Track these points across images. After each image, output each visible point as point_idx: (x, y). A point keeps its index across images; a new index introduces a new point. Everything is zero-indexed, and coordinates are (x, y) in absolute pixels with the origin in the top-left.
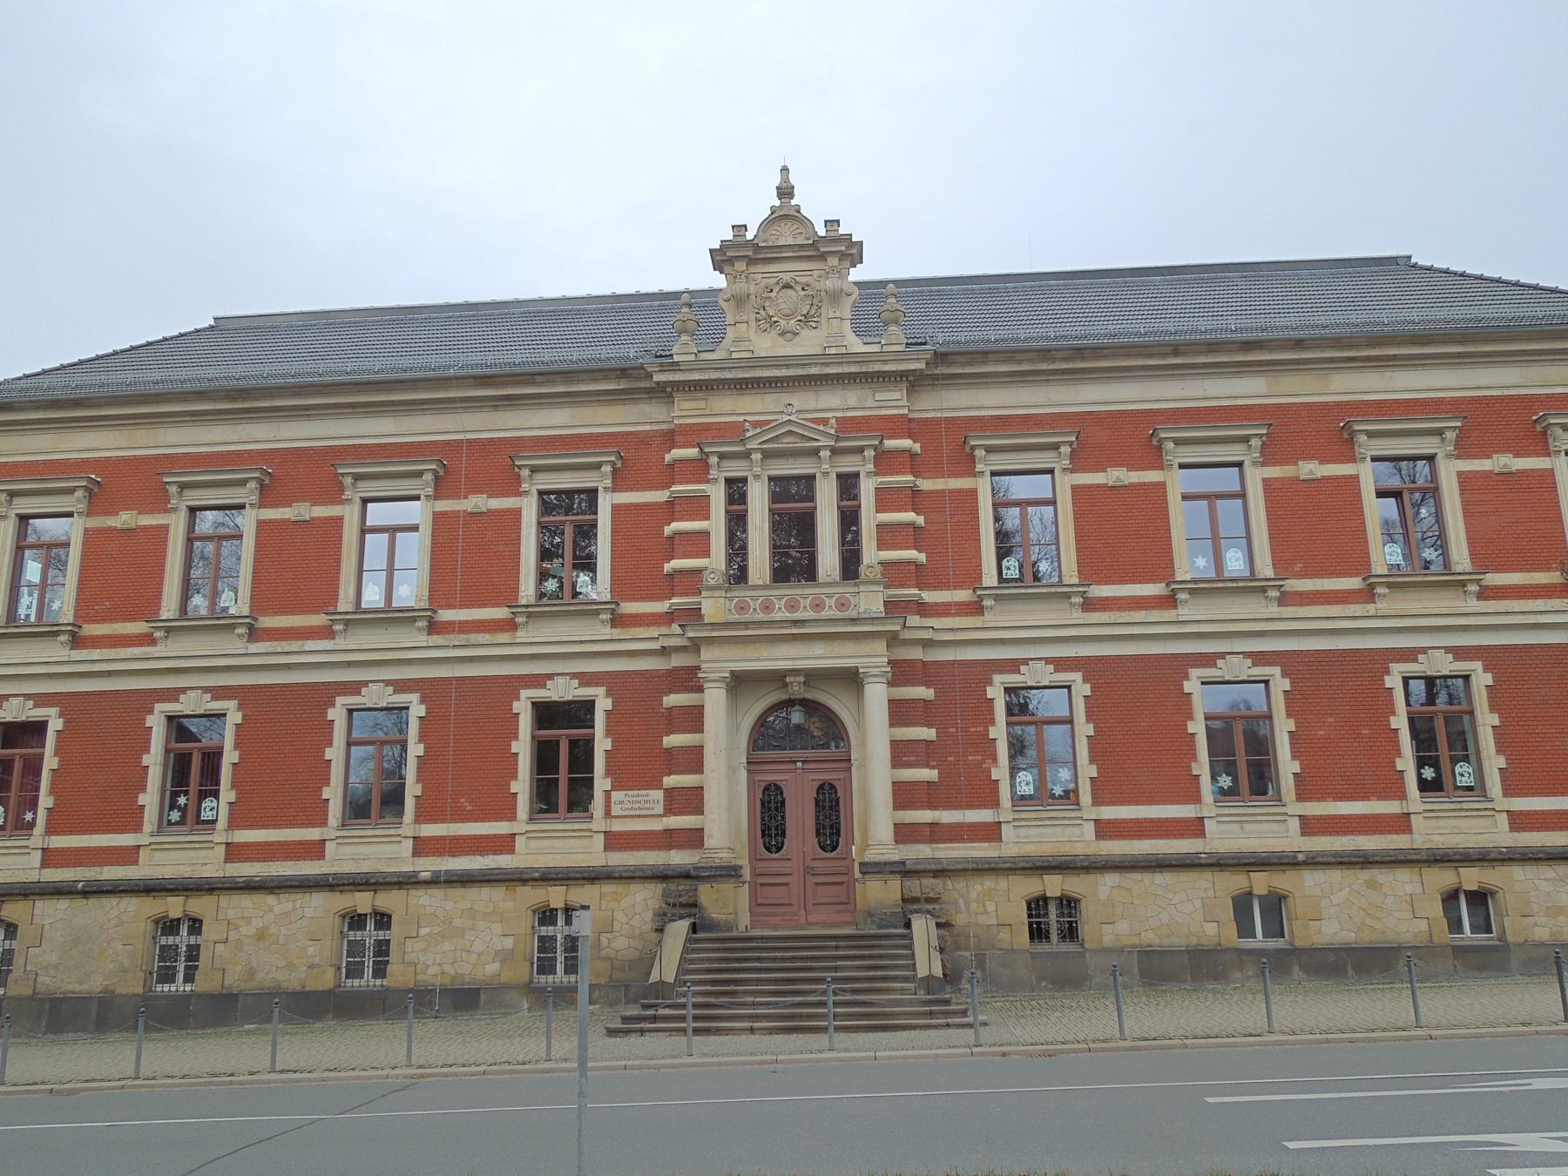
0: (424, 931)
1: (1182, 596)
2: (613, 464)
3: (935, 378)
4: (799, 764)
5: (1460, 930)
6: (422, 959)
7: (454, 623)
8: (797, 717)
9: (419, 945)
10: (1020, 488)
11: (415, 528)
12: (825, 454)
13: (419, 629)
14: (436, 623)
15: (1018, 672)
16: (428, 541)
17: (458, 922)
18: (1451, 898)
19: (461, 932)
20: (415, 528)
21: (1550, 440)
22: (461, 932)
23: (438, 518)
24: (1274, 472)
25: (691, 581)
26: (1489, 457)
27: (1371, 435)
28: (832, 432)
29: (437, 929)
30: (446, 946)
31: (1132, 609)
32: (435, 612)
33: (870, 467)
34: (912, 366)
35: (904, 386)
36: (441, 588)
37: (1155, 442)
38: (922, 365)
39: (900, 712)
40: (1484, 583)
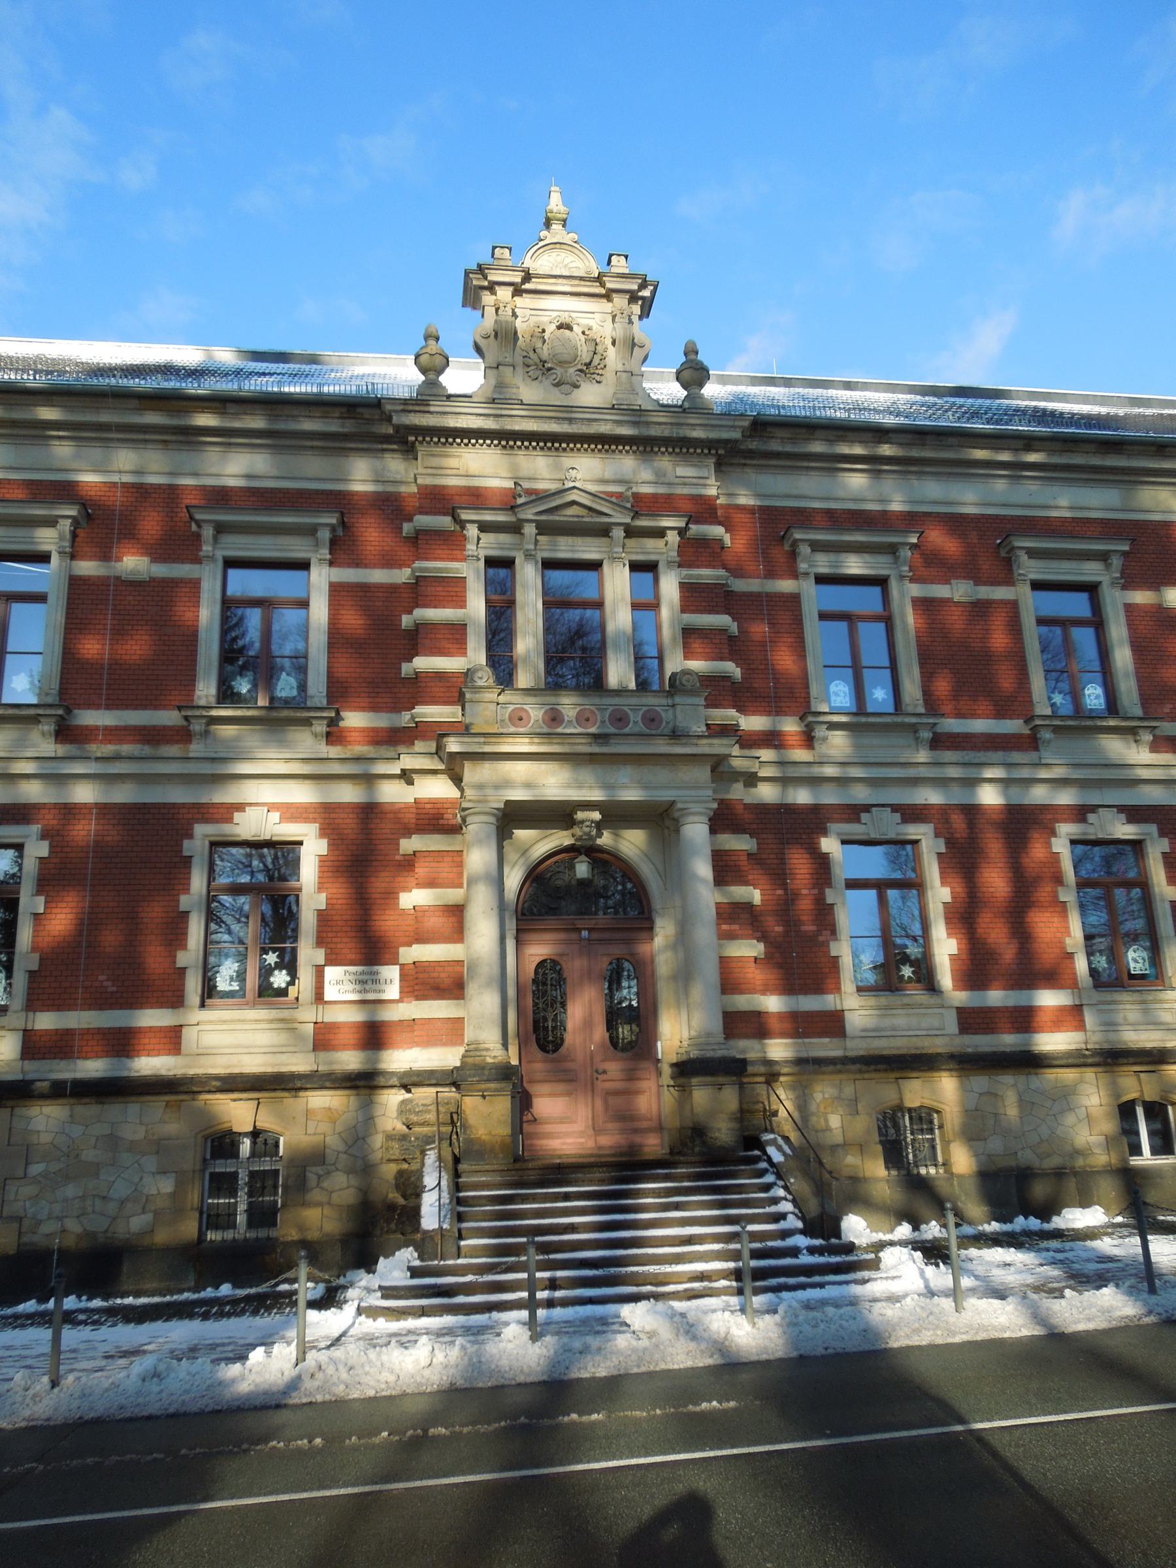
0: (36, 1169)
1: (1046, 735)
2: (333, 528)
3: (750, 454)
4: (585, 934)
5: (1136, 1150)
6: (31, 1211)
7: (97, 728)
8: (582, 869)
9: (28, 1190)
10: (244, 583)
11: (40, 598)
12: (618, 533)
13: (316, 735)
14: (69, 728)
15: (858, 821)
16: (60, 617)
17: (89, 1155)
18: (1126, 1111)
19: (94, 1170)
20: (40, 598)
21: (1015, 568)
22: (94, 1170)
23: (76, 584)
24: (1141, 597)
25: (455, 689)
26: (947, 582)
27: (1033, 553)
28: (629, 505)
29: (55, 1167)
30: (71, 1191)
31: (987, 749)
32: (69, 711)
33: (325, 553)
34: (725, 435)
35: (711, 462)
36: (75, 683)
37: (1003, 554)
38: (736, 435)
39: (726, 869)
40: (939, 729)
